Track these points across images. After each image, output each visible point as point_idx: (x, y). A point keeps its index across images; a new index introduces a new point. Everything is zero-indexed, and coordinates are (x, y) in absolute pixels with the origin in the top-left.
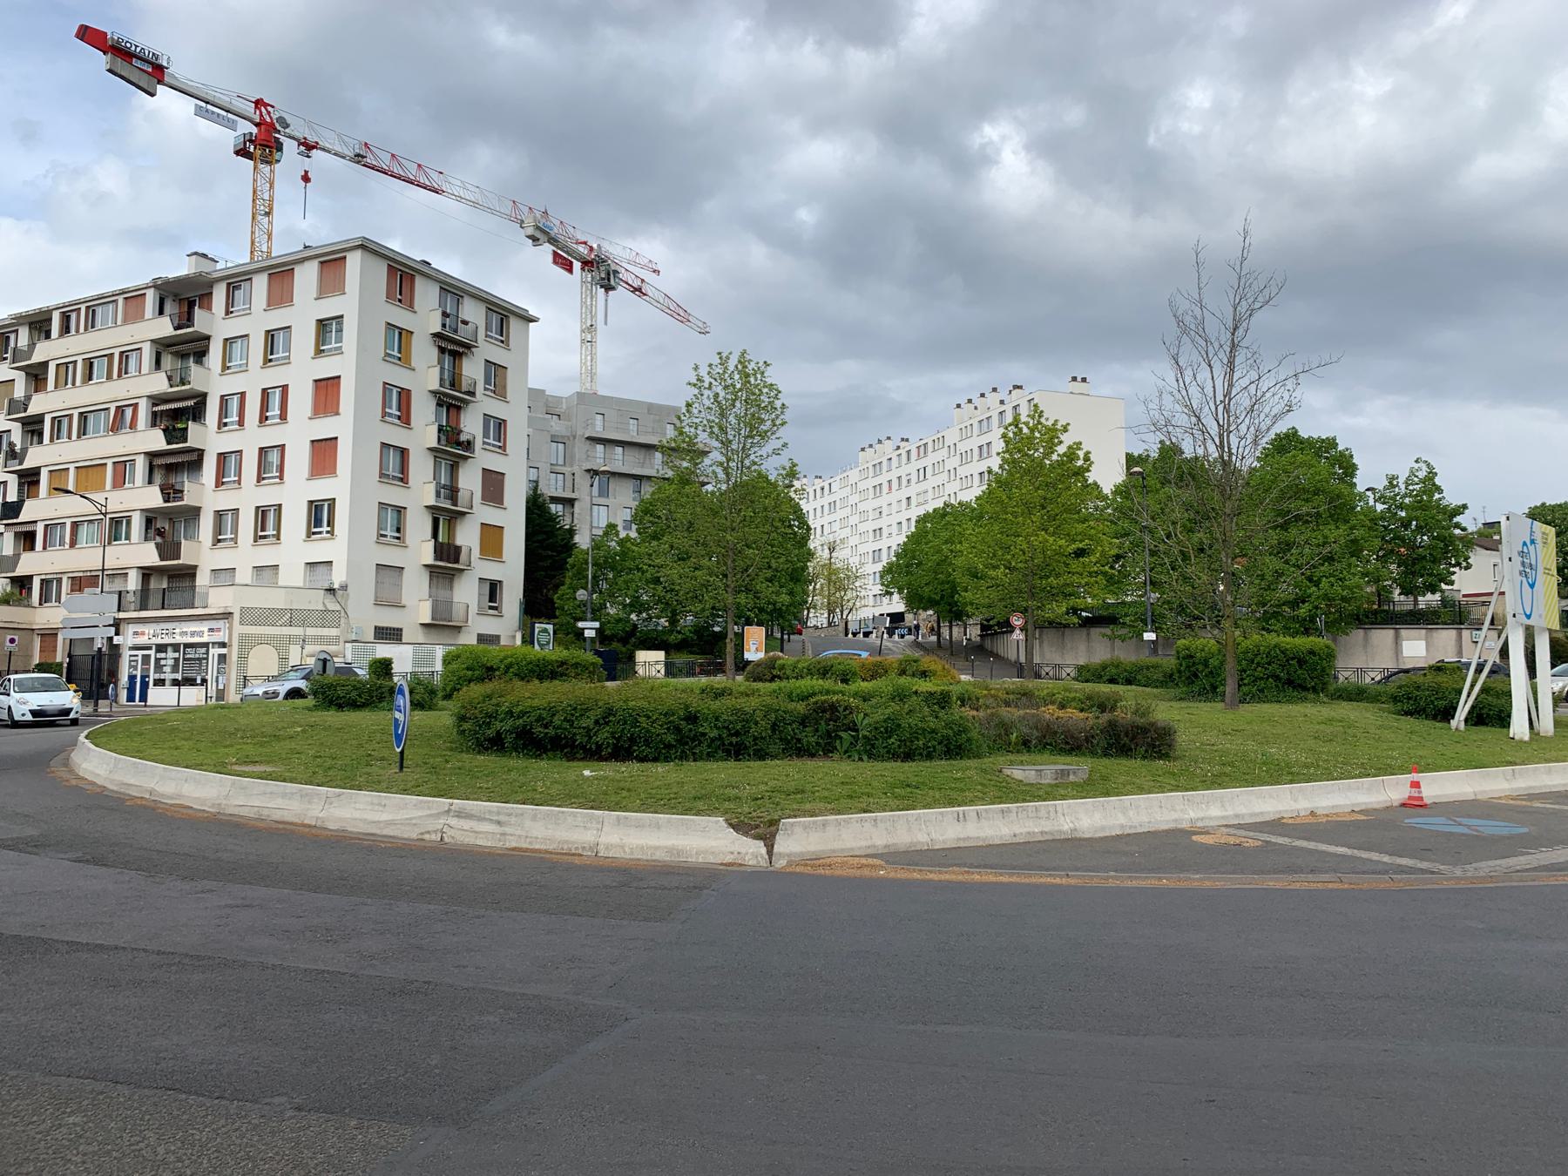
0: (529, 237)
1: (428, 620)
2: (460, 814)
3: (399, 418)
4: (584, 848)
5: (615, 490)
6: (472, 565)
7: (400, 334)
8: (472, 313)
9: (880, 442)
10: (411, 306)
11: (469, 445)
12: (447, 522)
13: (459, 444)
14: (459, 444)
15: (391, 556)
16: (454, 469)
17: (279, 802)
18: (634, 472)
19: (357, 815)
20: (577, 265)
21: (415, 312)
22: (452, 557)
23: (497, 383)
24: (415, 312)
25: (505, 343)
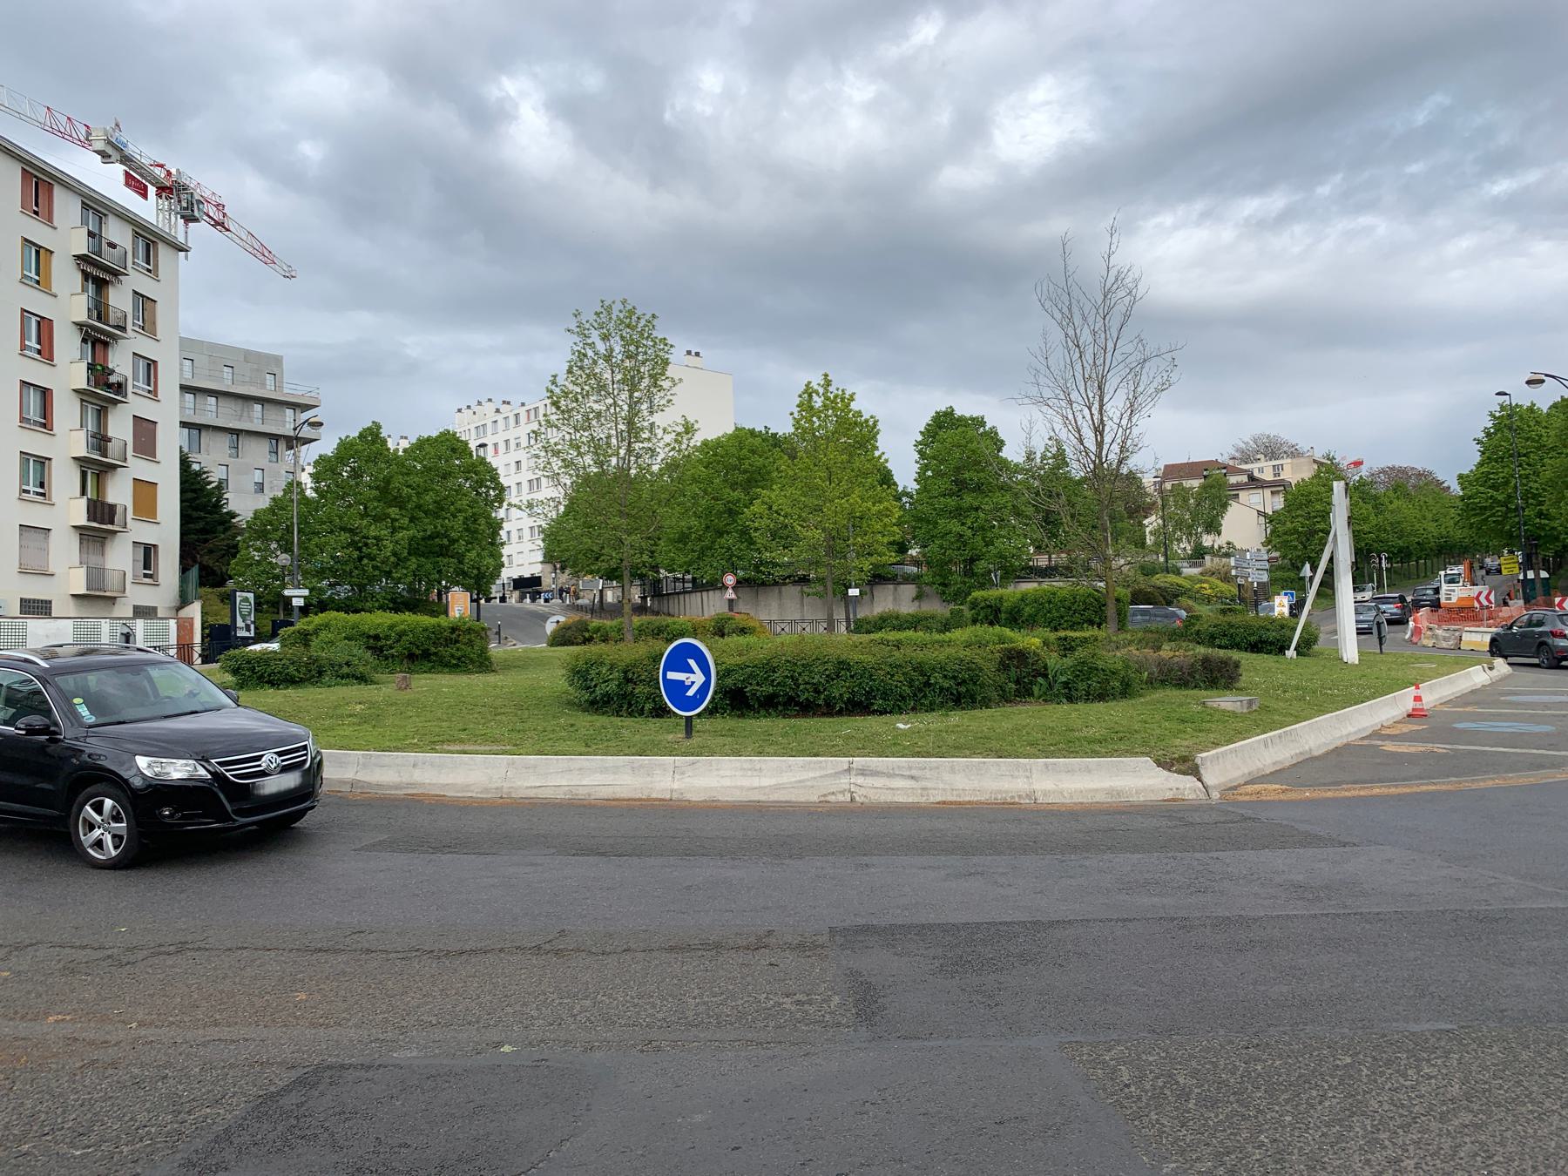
0: (98, 152)
1: (83, 591)
2: (863, 772)
3: (39, 352)
4: (1020, 796)
5: (208, 445)
6: (128, 526)
7: (37, 253)
8: (116, 232)
9: (479, 403)
10: (50, 219)
11: (120, 388)
12: (95, 477)
13: (109, 386)
14: (109, 386)
15: (36, 515)
16: (102, 414)
17: (608, 779)
18: (231, 425)
19: (727, 782)
20: (152, 190)
21: (55, 228)
22: (106, 517)
23: (146, 318)
24: (55, 228)
25: (153, 272)
